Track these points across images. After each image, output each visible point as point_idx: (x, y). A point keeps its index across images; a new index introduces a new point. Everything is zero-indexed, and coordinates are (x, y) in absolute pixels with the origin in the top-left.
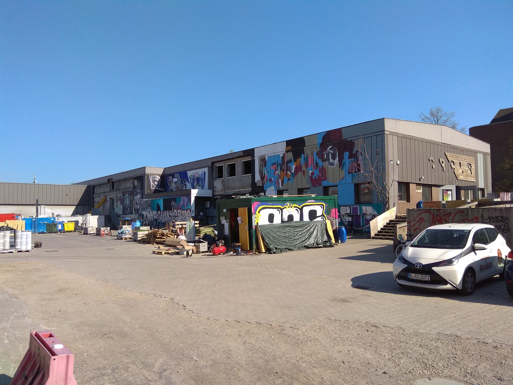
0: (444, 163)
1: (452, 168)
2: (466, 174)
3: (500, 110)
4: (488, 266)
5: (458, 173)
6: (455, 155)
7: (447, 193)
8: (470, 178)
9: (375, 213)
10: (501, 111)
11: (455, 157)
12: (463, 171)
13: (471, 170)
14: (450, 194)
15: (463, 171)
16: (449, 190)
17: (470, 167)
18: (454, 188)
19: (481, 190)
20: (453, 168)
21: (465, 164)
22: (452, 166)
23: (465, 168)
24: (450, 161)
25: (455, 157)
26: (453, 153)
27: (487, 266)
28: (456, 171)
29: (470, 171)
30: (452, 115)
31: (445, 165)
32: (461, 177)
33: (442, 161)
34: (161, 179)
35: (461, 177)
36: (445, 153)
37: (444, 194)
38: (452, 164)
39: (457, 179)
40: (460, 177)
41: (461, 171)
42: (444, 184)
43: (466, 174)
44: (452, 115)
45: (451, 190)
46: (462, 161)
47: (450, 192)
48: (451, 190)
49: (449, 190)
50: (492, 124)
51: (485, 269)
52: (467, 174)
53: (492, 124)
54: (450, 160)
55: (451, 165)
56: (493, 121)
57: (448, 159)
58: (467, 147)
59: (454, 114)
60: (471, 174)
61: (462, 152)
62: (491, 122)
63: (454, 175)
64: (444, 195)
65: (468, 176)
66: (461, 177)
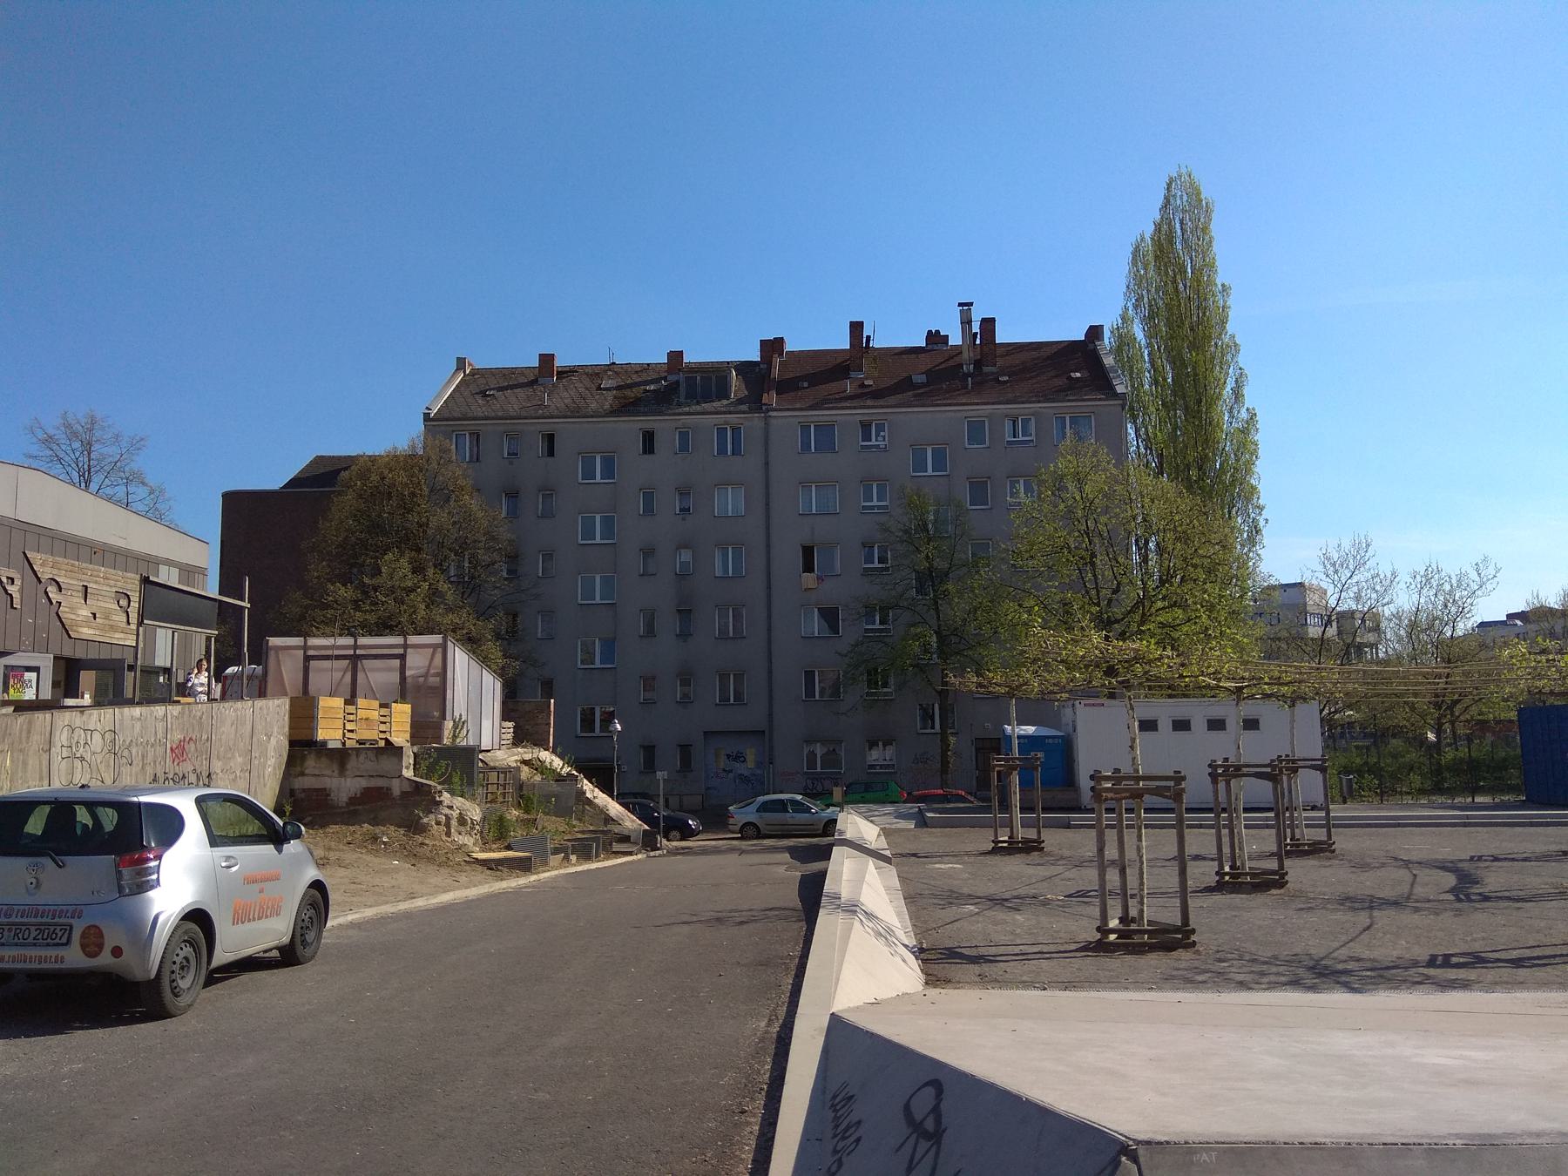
0: (18, 582)
1: (51, 603)
2: (107, 622)
3: (317, 456)
4: (268, 908)
5: (73, 617)
6: (66, 561)
7: (22, 676)
8: (122, 635)
9: (301, 783)
10: (319, 460)
11: (65, 567)
12: (94, 615)
13: (127, 612)
14: (30, 681)
15: (94, 615)
16: (29, 669)
17: (124, 602)
18: (46, 662)
19: (164, 673)
20: (54, 602)
21: (107, 594)
22: (50, 594)
23: (102, 604)
24: (43, 581)
25: (65, 567)
26: (74, 560)
27: (261, 907)
28: (65, 612)
29: (125, 615)
30: (138, 445)
31: (21, 591)
32: (87, 632)
33: (8, 578)
34: (1067, 346)
35: (85, 630)
36: (24, 553)
37: (11, 680)
38: (52, 590)
39: (70, 637)
40: (81, 630)
41: (85, 612)
42: (9, 648)
43: (107, 622)
44: (137, 445)
45: (36, 669)
46: (96, 582)
47: (34, 675)
48: (36, 669)
49: (29, 669)
50: (284, 490)
51: (254, 920)
52: (111, 623)
53: (284, 490)
54: (44, 577)
55: (46, 593)
56: (293, 483)
57: (34, 572)
58: (121, 544)
59: (142, 443)
60: (129, 623)
61: (99, 555)
62: (285, 486)
63: (59, 623)
64: (11, 682)
65: (113, 628)
66: (85, 630)
